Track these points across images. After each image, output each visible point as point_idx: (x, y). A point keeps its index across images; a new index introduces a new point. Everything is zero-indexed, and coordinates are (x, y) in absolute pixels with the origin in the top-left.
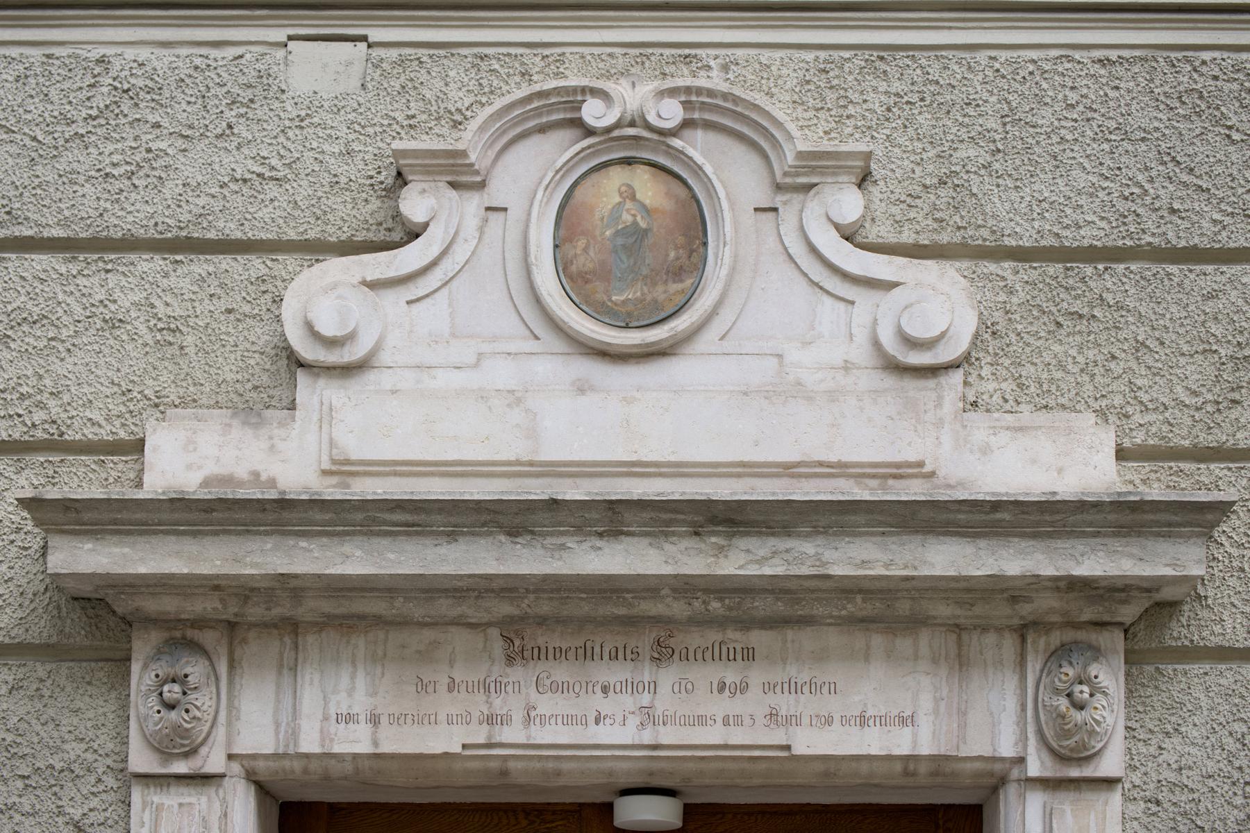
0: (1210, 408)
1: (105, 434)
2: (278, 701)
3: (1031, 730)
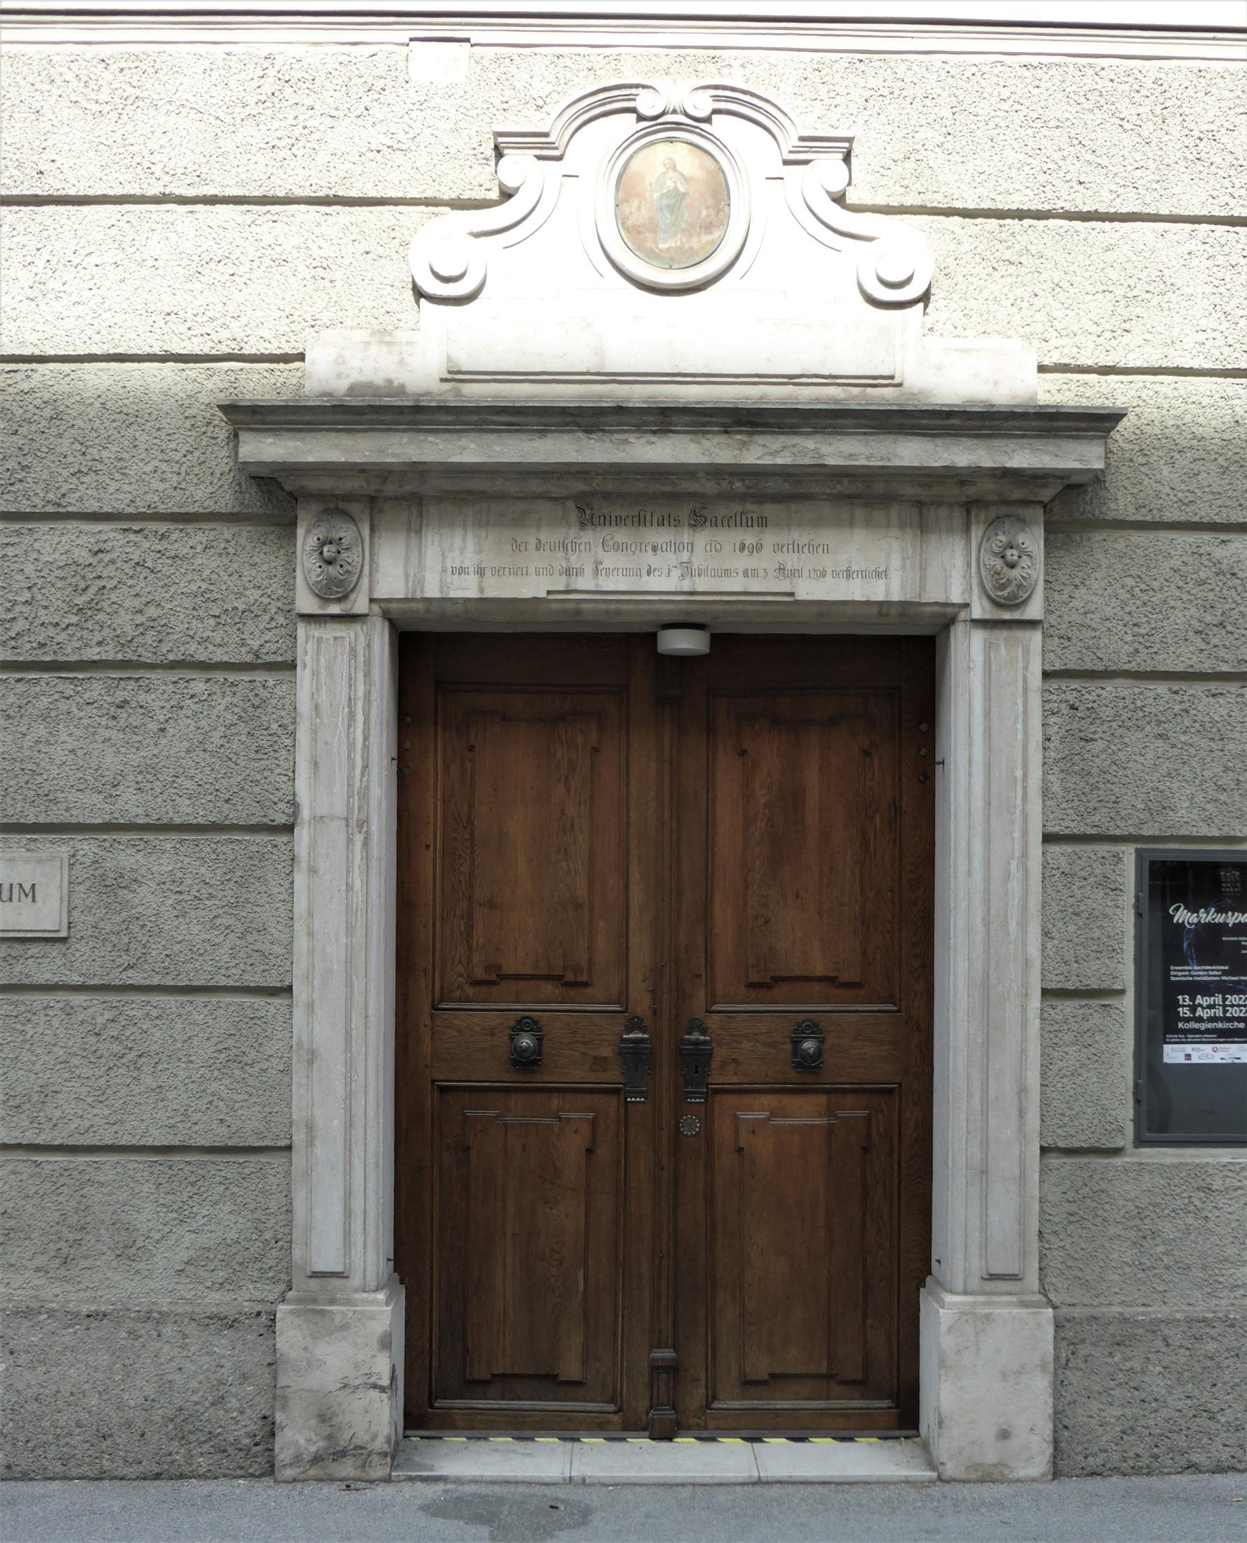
2: (407, 557)
3: (975, 581)
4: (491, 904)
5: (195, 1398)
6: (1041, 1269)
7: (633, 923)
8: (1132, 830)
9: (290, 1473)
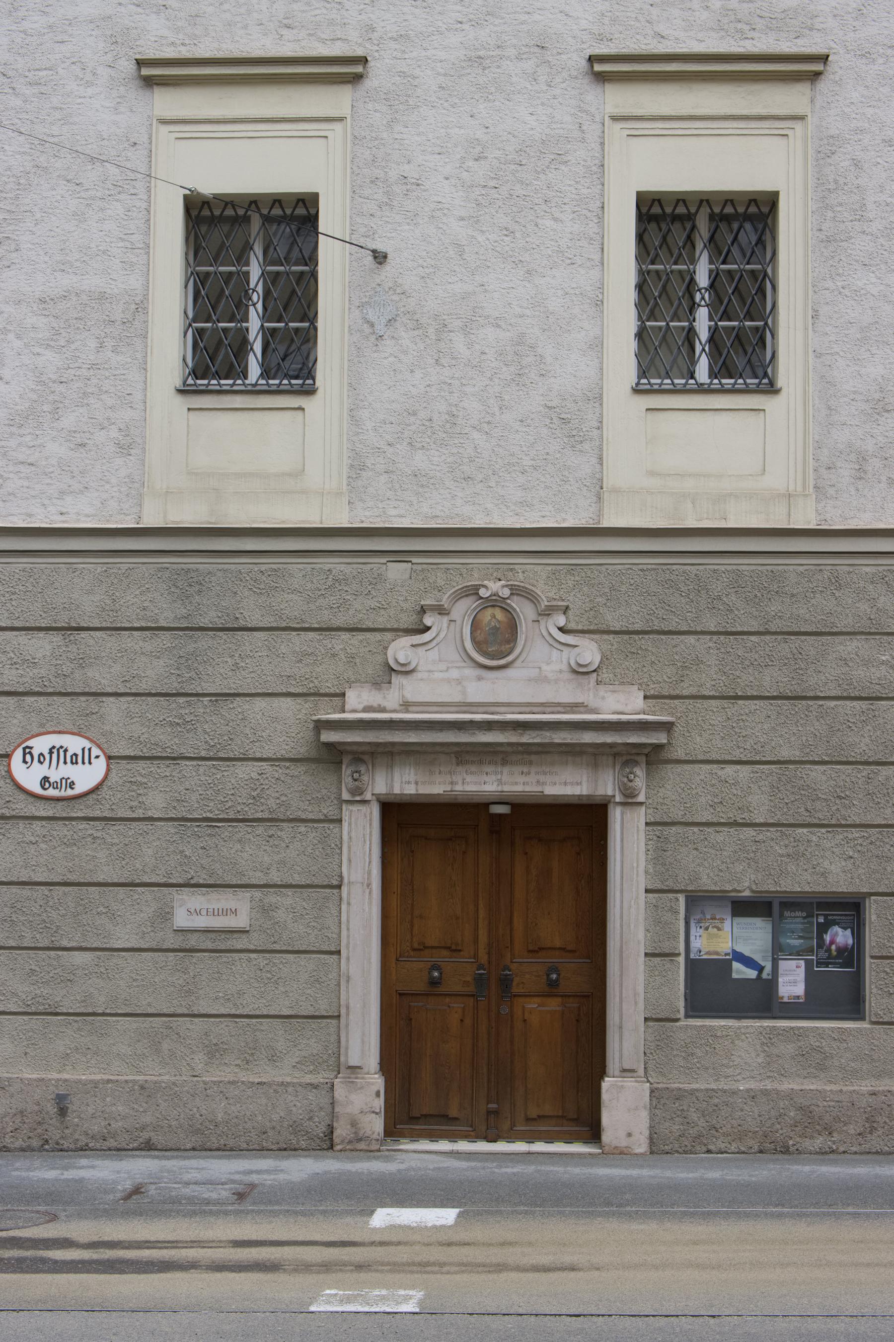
0: (674, 683)
1: (332, 691)
2: (387, 777)
3: (617, 787)
4: (421, 917)
5: (301, 1117)
6: (645, 1068)
7: (480, 926)
8: (683, 888)
9: (339, 1147)
